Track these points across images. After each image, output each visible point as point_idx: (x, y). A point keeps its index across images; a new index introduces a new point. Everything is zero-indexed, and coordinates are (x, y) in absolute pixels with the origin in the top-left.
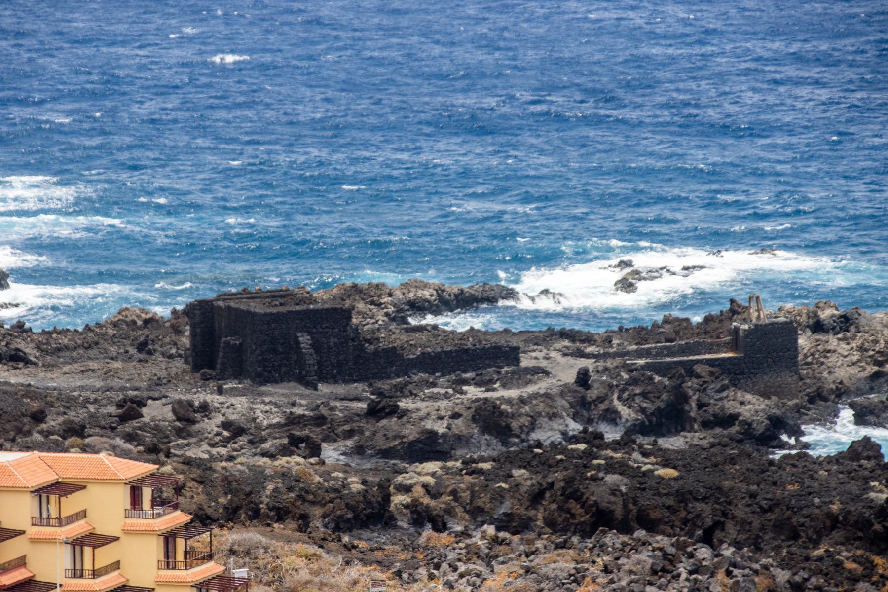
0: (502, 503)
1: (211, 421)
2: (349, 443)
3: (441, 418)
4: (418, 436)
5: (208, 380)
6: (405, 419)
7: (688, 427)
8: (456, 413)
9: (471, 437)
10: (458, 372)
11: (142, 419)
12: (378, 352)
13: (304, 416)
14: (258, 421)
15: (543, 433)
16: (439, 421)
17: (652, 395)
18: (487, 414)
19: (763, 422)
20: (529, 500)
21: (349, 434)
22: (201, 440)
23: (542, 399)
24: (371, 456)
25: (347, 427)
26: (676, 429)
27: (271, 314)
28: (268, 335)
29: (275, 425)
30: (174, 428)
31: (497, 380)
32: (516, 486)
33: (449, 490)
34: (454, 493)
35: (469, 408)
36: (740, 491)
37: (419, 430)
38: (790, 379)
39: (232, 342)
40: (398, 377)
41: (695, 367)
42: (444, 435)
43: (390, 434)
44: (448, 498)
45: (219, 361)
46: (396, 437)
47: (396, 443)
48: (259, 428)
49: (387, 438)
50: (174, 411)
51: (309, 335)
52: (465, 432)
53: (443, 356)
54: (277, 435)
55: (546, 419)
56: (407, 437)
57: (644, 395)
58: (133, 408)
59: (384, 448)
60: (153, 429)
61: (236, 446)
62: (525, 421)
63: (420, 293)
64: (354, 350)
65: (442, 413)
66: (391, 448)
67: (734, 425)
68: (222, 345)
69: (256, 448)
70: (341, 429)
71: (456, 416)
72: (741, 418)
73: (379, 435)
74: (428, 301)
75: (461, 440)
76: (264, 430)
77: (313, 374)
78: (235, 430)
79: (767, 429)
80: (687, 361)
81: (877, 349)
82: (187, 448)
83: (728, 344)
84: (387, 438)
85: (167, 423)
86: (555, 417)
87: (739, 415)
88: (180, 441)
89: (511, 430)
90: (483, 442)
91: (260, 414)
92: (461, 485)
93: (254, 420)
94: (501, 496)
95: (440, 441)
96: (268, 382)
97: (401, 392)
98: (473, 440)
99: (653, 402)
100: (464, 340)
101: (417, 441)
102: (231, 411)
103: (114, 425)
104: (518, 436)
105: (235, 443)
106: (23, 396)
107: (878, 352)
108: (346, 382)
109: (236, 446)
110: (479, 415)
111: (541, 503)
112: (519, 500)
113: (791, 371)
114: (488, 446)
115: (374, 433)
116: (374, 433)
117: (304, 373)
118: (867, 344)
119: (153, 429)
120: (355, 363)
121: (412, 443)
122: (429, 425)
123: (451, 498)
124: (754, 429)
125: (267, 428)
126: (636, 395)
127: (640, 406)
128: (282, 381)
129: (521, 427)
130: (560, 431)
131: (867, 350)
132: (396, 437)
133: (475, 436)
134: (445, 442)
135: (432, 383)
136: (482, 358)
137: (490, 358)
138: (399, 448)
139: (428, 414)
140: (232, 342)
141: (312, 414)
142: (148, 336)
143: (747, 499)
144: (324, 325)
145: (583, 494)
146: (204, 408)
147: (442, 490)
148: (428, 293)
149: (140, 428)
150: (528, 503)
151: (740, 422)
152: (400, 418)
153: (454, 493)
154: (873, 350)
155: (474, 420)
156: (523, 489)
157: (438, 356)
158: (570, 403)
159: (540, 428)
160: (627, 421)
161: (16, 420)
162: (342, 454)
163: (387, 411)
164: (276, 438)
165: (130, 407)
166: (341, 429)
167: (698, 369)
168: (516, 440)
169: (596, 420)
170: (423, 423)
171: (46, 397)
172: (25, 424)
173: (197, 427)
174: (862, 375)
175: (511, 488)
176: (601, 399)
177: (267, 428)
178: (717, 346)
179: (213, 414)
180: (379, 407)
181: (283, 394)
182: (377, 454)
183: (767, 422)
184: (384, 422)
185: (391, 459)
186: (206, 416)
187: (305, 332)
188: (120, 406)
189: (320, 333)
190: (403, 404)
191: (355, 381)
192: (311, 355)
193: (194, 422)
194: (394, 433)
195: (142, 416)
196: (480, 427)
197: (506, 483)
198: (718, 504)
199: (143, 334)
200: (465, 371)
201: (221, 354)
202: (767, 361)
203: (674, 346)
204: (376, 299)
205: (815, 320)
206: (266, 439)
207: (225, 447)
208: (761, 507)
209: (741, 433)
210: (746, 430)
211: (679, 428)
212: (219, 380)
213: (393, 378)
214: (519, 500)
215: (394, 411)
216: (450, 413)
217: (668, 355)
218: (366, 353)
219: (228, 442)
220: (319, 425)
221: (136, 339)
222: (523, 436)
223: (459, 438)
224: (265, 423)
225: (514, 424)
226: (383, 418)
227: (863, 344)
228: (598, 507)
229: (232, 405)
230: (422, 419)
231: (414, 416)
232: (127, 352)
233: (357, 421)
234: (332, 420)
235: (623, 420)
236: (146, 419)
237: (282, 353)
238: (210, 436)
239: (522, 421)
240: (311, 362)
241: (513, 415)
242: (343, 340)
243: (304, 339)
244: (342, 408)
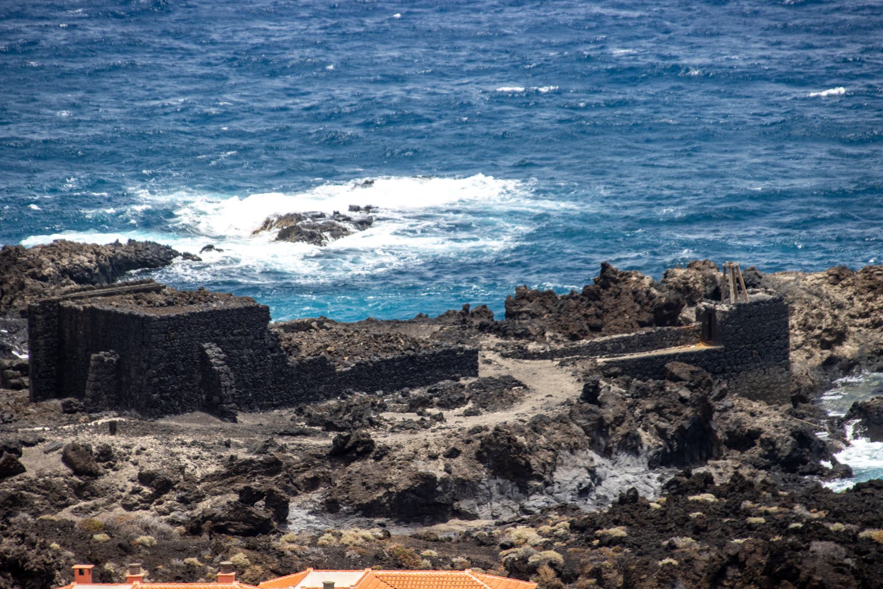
3: (433, 457)
4: (410, 483)
5: (74, 412)
6: (385, 460)
8: (454, 449)
9: (479, 482)
11: (25, 474)
14: (186, 470)
15: (566, 473)
16: (432, 462)
19: (788, 440)
21: (312, 484)
22: (112, 501)
25: (309, 474)
28: (165, 348)
29: (212, 476)
30: (71, 484)
31: (468, 399)
32: (687, 561)
33: (589, 568)
34: (596, 573)
37: (412, 475)
38: (780, 377)
39: (106, 359)
42: (444, 481)
43: (372, 482)
46: (380, 485)
47: (380, 494)
48: (190, 479)
49: (368, 488)
51: (218, 346)
52: (470, 476)
53: (384, 367)
54: (218, 490)
55: (567, 453)
57: (658, 410)
58: (13, 460)
59: (365, 501)
60: (43, 488)
61: (162, 507)
65: (434, 449)
66: (374, 501)
67: (754, 445)
68: (92, 363)
69: (191, 509)
70: (300, 477)
71: (453, 453)
72: (763, 436)
73: (356, 484)
74: (88, 270)
76: (199, 483)
77: (230, 400)
78: (157, 485)
79: (794, 450)
81: (824, 326)
82: (94, 513)
83: (698, 331)
87: (759, 431)
88: (82, 503)
90: (494, 488)
91: (188, 461)
92: (606, 562)
93: (182, 469)
94: (672, 577)
95: (439, 489)
96: (166, 413)
97: (360, 421)
98: (481, 486)
99: (670, 420)
101: (410, 490)
104: (540, 478)
105: (160, 503)
107: (826, 330)
109: (162, 507)
114: (502, 493)
115: (349, 481)
116: (349, 481)
117: (216, 399)
118: (811, 320)
119: (43, 488)
121: (402, 494)
122: (422, 466)
123: (594, 581)
124: (779, 450)
125: (203, 481)
126: (648, 411)
127: (656, 426)
128: (184, 411)
129: (543, 466)
131: (811, 328)
132: (380, 485)
134: (445, 490)
137: (441, 367)
140: (106, 359)
141: (261, 459)
146: (106, 454)
147: (578, 570)
148: (86, 259)
149: (24, 488)
151: (762, 441)
152: (377, 459)
154: (820, 328)
155: (479, 457)
156: (700, 566)
158: (583, 428)
159: (562, 464)
160: (649, 448)
162: (310, 513)
164: (216, 494)
165: (8, 458)
166: (300, 477)
167: (676, 368)
168: (539, 484)
169: (615, 450)
173: (101, 482)
174: (811, 362)
175: (680, 564)
176: (619, 420)
177: (203, 481)
178: (685, 334)
179: (119, 463)
180: (349, 444)
182: (356, 511)
183: (791, 438)
184: (356, 466)
186: (111, 466)
187: (213, 342)
189: (231, 342)
190: (380, 439)
191: (276, 407)
193: (95, 475)
194: (376, 481)
195: (22, 469)
197: (672, 556)
200: (412, 387)
201: (91, 376)
202: (752, 353)
203: (633, 337)
204: (36, 270)
205: (713, 288)
206: (204, 496)
207: (147, 509)
209: (766, 457)
210: (770, 451)
211: (704, 455)
212: (91, 412)
213: (322, 401)
215: (366, 449)
216: (443, 449)
217: (626, 351)
218: (288, 366)
219: (151, 503)
220: (271, 473)
222: (547, 477)
224: (199, 474)
231: (396, 454)
235: (645, 448)
236: (31, 474)
237: (183, 373)
238: (124, 494)
239: (542, 456)
240: (228, 383)
242: (260, 351)
243: (213, 351)
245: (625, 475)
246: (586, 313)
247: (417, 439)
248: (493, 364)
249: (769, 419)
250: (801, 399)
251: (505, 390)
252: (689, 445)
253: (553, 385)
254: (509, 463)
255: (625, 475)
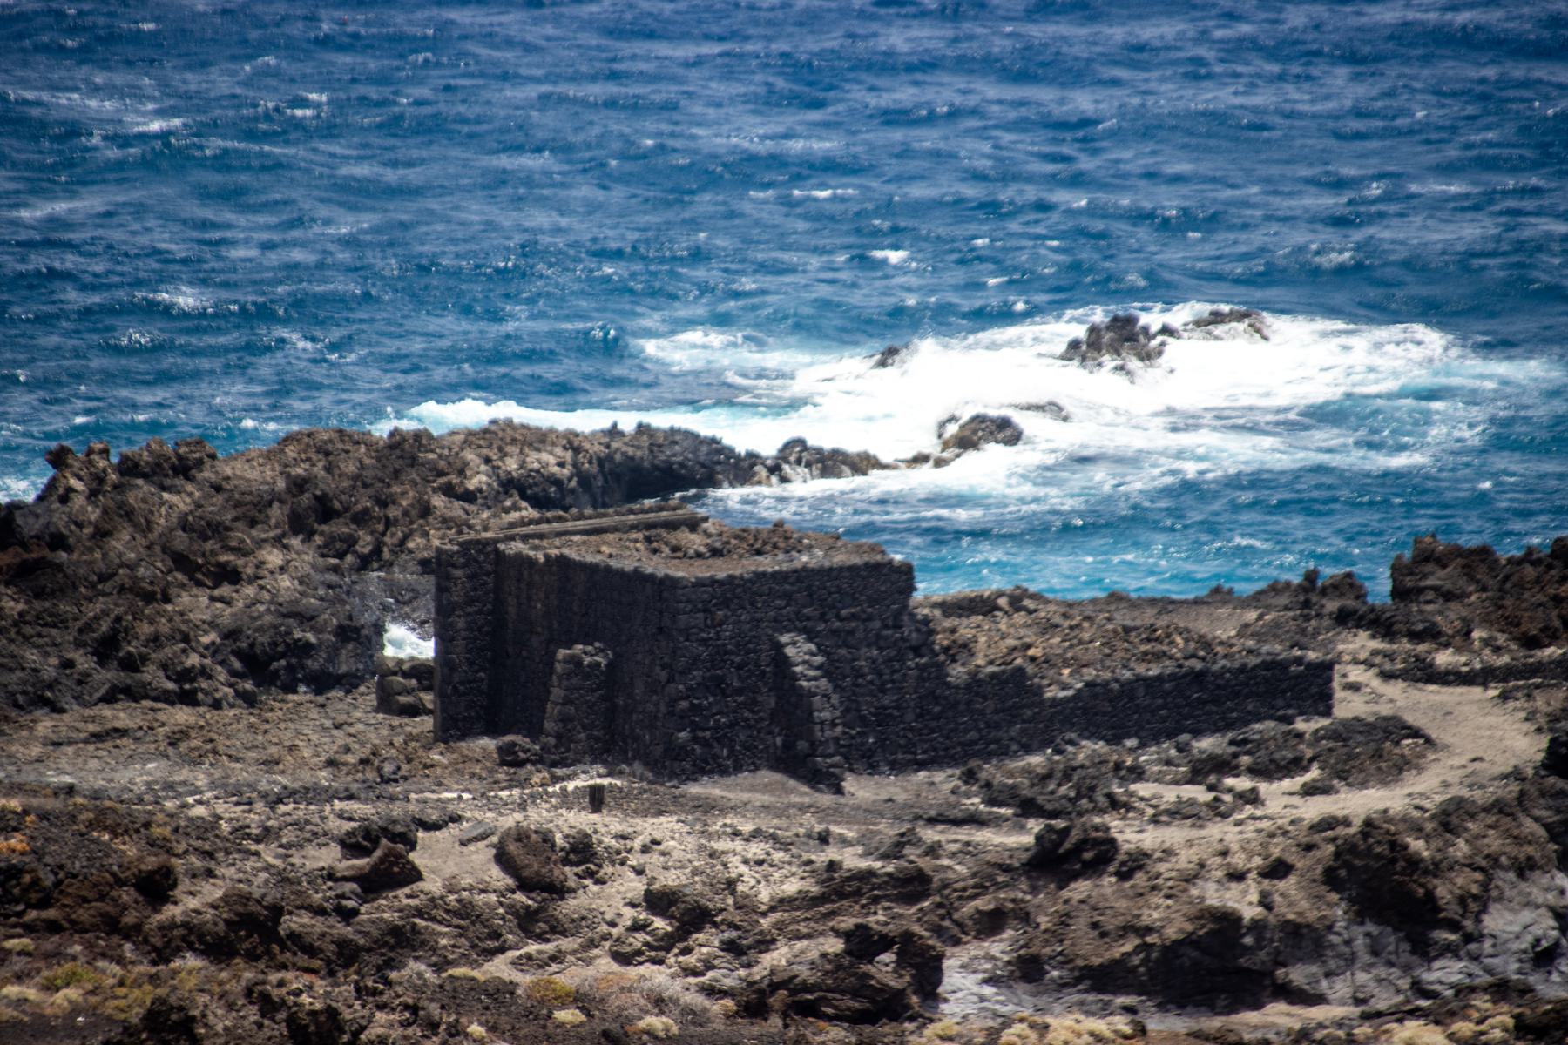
1: (608, 889)
2: (1000, 947)
3: (1237, 876)
4: (1189, 927)
5: (520, 764)
6: (1140, 879)
9: (1330, 928)
10: (1184, 737)
11: (421, 885)
12: (980, 683)
13: (871, 873)
14: (740, 888)
15: (1509, 916)
16: (1233, 885)
21: (991, 924)
22: (592, 944)
23: (1491, 819)
24: (1062, 986)
25: (984, 903)
27: (713, 582)
28: (704, 642)
30: (511, 909)
31: (1311, 760)
35: (1309, 847)
39: (587, 660)
42: (1257, 926)
43: (1110, 923)
45: (551, 709)
46: (1127, 930)
48: (746, 906)
49: (1103, 935)
50: (503, 858)
51: (810, 640)
53: (1141, 692)
55: (1511, 876)
56: (1158, 930)
59: (1097, 961)
60: (456, 914)
62: (1465, 880)
63: (534, 459)
64: (921, 679)
65: (1238, 860)
68: (559, 667)
69: (748, 966)
70: (968, 908)
71: (1278, 870)
73: (1079, 925)
74: (557, 482)
75: (1303, 939)
76: (764, 914)
82: (555, 967)
84: (1103, 935)
85: (493, 898)
88: (533, 947)
90: (1360, 943)
91: (743, 869)
93: (731, 885)
95: (1248, 940)
96: (703, 772)
97: (1091, 800)
98: (1334, 939)
101: (1188, 941)
102: (654, 859)
103: (350, 904)
104: (1454, 926)
105: (687, 951)
106: (90, 825)
108: (898, 768)
109: (691, 960)
114: (1375, 953)
115: (1064, 920)
116: (1064, 920)
119: (456, 914)
120: (920, 716)
122: (1214, 894)
125: (772, 909)
128: (738, 768)
130: (1552, 909)
132: (1127, 930)
134: (1259, 945)
135: (1131, 770)
138: (1136, 960)
139: (1202, 865)
140: (587, 660)
141: (890, 869)
142: (118, 619)
144: (844, 612)
146: (582, 851)
148: (552, 460)
149: (420, 913)
152: (1123, 876)
155: (1331, 879)
158: (1546, 826)
161: (102, 897)
163: (1088, 855)
166: (968, 908)
168: (1452, 937)
170: (1194, 892)
171: (147, 825)
172: (125, 908)
173: (571, 906)
177: (772, 909)
179: (608, 869)
180: (1067, 845)
181: (765, 808)
182: (1078, 981)
184: (1080, 889)
185: (1114, 993)
186: (590, 874)
187: (800, 631)
188: (351, 846)
189: (835, 632)
190: (1130, 835)
191: (921, 765)
192: (826, 696)
193: (560, 891)
194: (1120, 921)
195: (415, 875)
196: (1351, 901)
199: (105, 613)
204: (454, 479)
206: (774, 941)
207: (660, 962)
212: (554, 764)
215: (1099, 855)
218: (948, 685)
220: (911, 899)
221: (87, 628)
222: (1468, 924)
224: (765, 895)
225: (1443, 892)
226: (1075, 877)
229: (656, 842)
230: (1189, 879)
232: (69, 664)
233: (1005, 885)
234: (945, 885)
236: (432, 885)
238: (615, 931)
239: (1460, 881)
240: (826, 715)
241: (1436, 865)
243: (799, 650)
244: (955, 847)
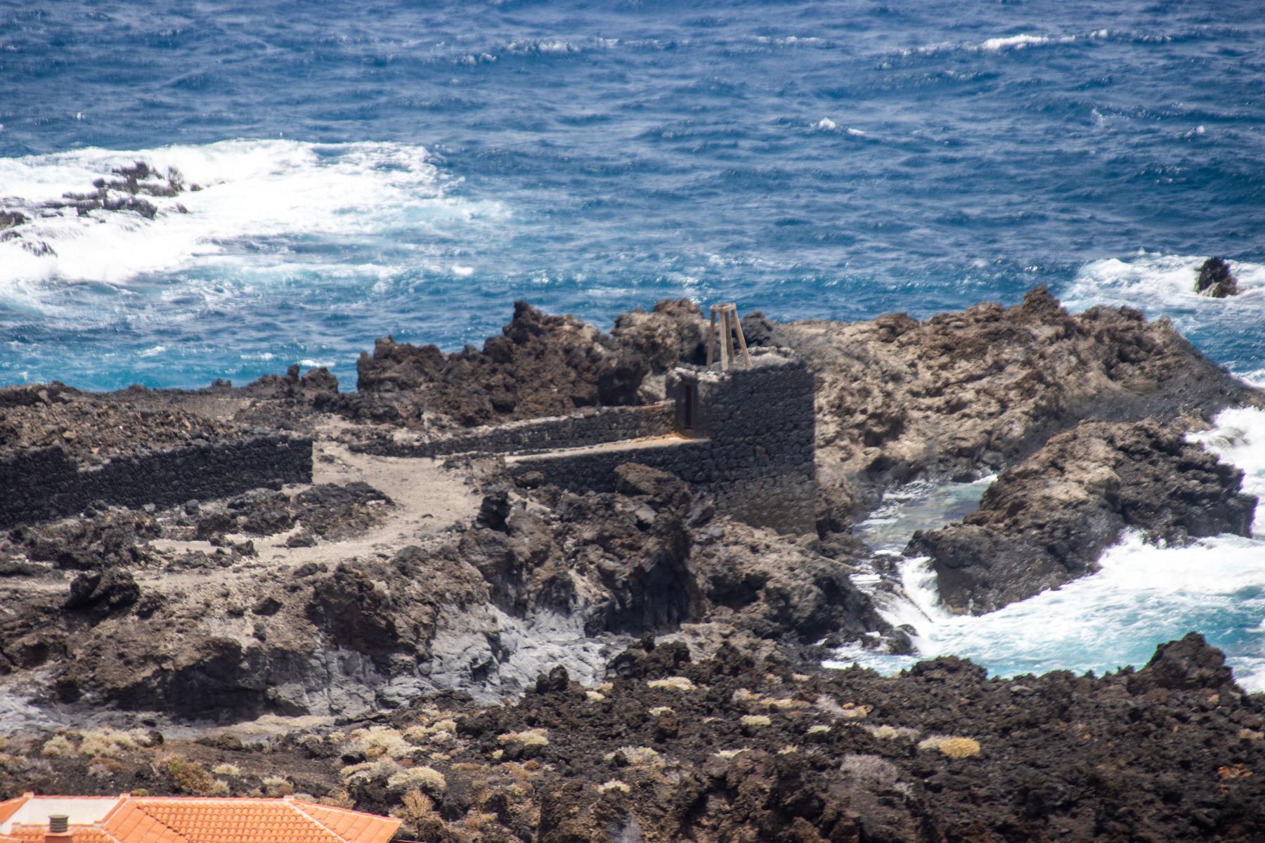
0: (622, 826)
2: (43, 675)
3: (236, 613)
4: (198, 655)
6: (157, 617)
7: (692, 609)
9: (310, 654)
10: (193, 502)
16: (234, 620)
17: (619, 541)
18: (345, 602)
19: (810, 592)
20: (679, 819)
21: (35, 656)
24: (93, 705)
25: (29, 640)
26: (669, 615)
32: (644, 786)
34: (498, 805)
35: (294, 589)
36: (1140, 787)
38: (799, 490)
40: (65, 514)
41: (620, 469)
42: (253, 653)
43: (134, 653)
44: (486, 817)
46: (147, 659)
47: (148, 673)
49: (128, 663)
52: (296, 645)
53: (157, 466)
55: (455, 608)
56: (172, 659)
57: (602, 541)
59: (122, 684)
62: (419, 613)
65: (237, 601)
66: (138, 685)
67: (756, 598)
70: (17, 643)
71: (269, 607)
73: (108, 655)
75: (289, 663)
80: (601, 456)
81: (870, 409)
83: (668, 414)
86: (470, 602)
89: (396, 636)
90: (335, 666)
95: (245, 665)
97: (117, 554)
100: (171, 424)
101: (198, 667)
104: (410, 649)
107: (873, 416)
110: (325, 603)
111: (699, 824)
112: (656, 818)
113: (801, 472)
115: (96, 651)
116: (96, 651)
118: (849, 399)
121: (184, 674)
122: (217, 628)
124: (795, 607)
126: (587, 543)
127: (599, 567)
130: (486, 634)
131: (850, 412)
132: (147, 659)
133: (318, 652)
135: (149, 529)
136: (234, 467)
137: (252, 467)
138: (155, 683)
143: (1159, 805)
145: (823, 804)
147: (468, 799)
150: (676, 825)
152: (144, 615)
153: (498, 805)
154: (864, 412)
155: (312, 614)
156: (664, 794)
157: (146, 464)
158: (481, 568)
159: (445, 627)
162: (31, 703)
166: (17, 643)
167: (633, 473)
168: (408, 658)
169: (531, 604)
170: (201, 627)
175: (634, 790)
180: (97, 591)
182: (107, 700)
184: (109, 626)
190: (149, 582)
194: (141, 651)
196: (327, 631)
198: (1116, 819)
202: (755, 451)
203: (565, 423)
205: (694, 345)
208: (1195, 821)
209: (775, 619)
210: (781, 610)
211: (676, 614)
213: (53, 519)
214: (656, 818)
215: (124, 599)
216: (253, 601)
217: (553, 444)
222: (421, 648)
223: (282, 656)
226: (104, 616)
227: (841, 398)
228: (862, 831)
230: (198, 617)
233: (48, 624)
235: (581, 602)
239: (413, 614)
245: (551, 646)
246: (489, 374)
247: (211, 583)
248: (336, 461)
249: (780, 558)
250: (832, 526)
251: (353, 506)
252: (652, 598)
253: (432, 499)
254: (359, 623)
255: (551, 646)
